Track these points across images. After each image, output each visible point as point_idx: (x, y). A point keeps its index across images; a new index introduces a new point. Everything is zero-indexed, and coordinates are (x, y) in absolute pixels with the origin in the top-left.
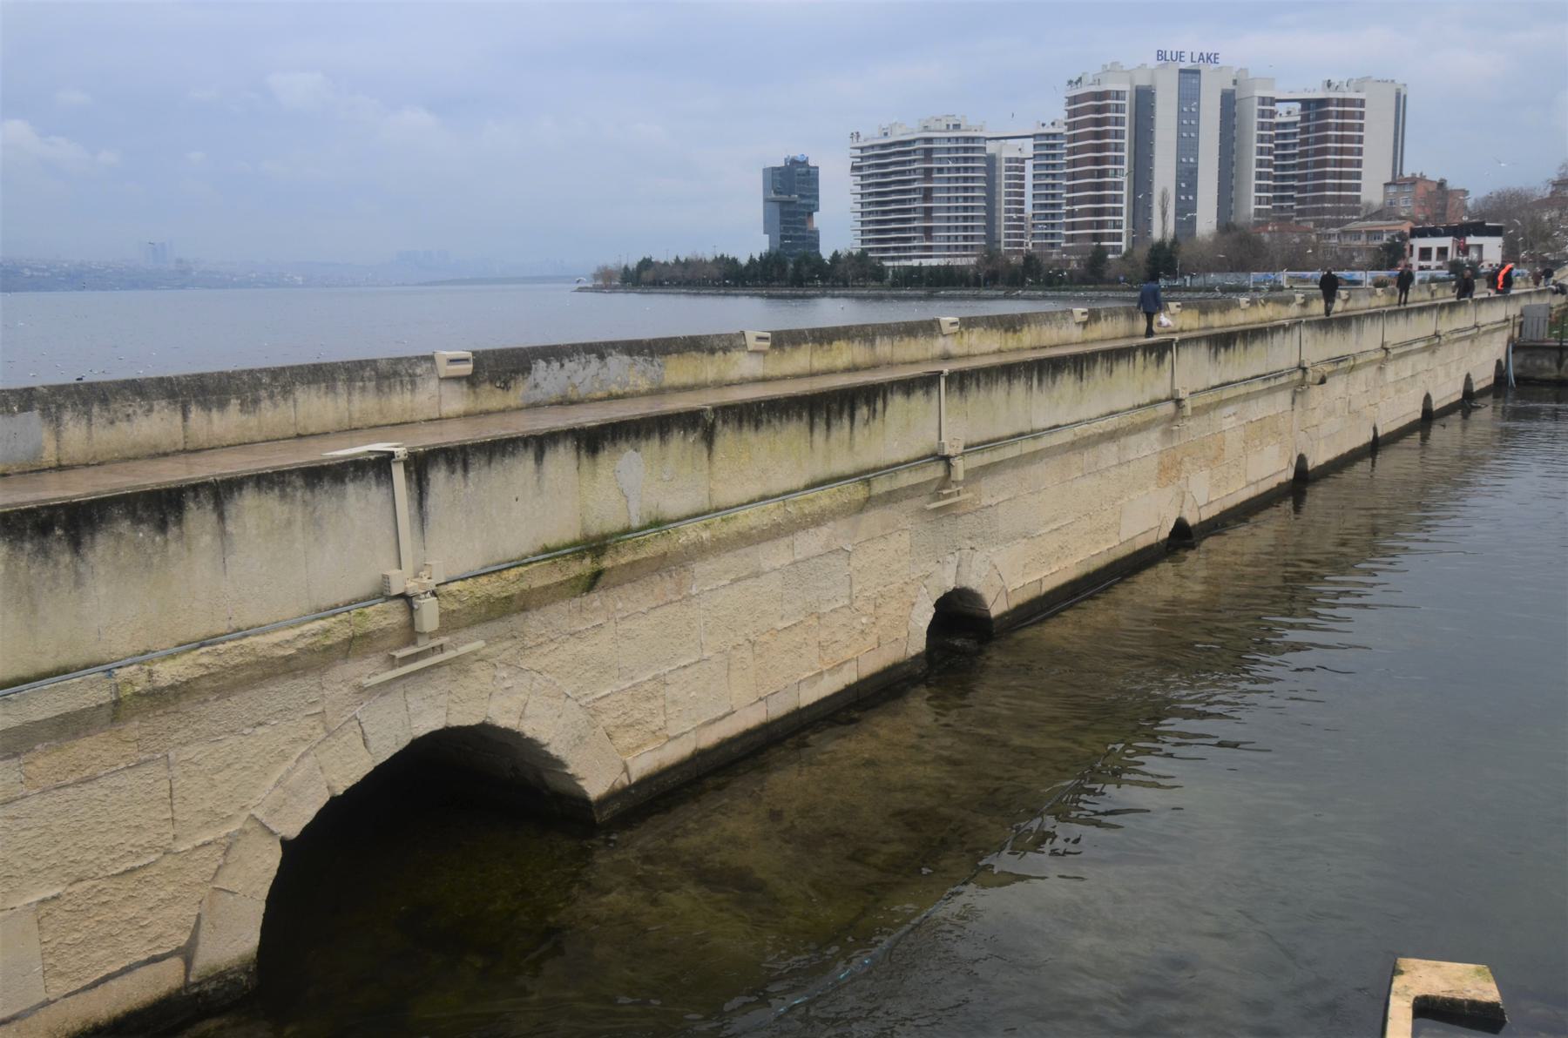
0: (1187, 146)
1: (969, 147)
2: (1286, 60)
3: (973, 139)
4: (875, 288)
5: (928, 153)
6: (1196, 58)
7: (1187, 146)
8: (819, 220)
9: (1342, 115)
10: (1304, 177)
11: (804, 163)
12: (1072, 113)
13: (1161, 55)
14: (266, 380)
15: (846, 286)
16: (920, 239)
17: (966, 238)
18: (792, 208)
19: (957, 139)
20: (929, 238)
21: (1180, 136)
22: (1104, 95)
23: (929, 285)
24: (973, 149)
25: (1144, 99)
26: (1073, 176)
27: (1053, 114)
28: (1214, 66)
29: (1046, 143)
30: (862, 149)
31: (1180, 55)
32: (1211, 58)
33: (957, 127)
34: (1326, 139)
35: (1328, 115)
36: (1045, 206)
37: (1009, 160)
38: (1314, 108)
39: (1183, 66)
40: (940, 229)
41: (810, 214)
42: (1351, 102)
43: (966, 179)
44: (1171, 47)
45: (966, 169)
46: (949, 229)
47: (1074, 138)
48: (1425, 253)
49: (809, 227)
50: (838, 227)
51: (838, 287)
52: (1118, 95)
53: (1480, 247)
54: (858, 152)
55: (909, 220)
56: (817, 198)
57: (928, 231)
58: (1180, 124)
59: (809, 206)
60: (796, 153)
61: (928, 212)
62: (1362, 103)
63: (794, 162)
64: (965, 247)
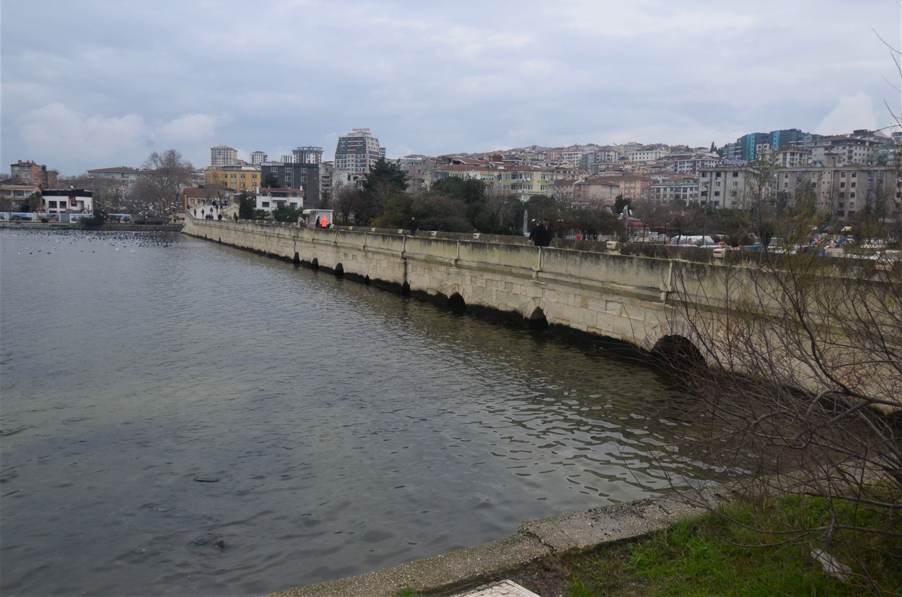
53: (82, 202)
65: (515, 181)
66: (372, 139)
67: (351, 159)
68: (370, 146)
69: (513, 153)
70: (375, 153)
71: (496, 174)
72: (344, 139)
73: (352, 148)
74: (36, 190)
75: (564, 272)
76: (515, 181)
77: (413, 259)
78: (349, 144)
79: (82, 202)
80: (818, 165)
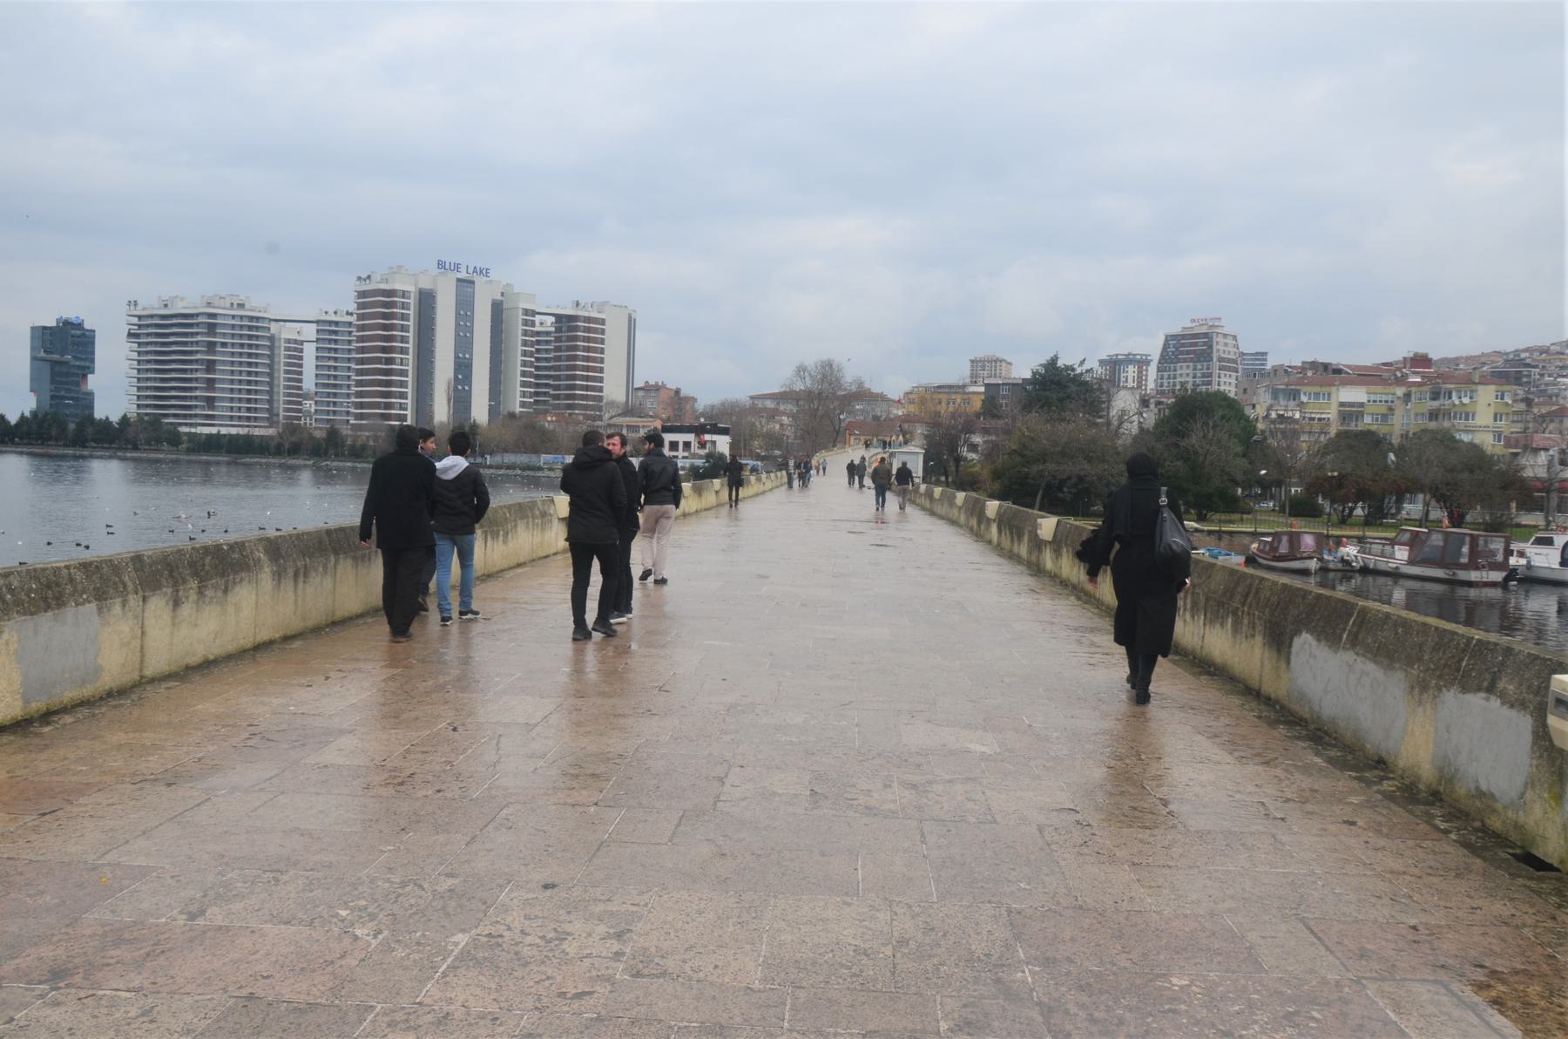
0: (464, 342)
1: (253, 329)
2: (547, 282)
3: (258, 319)
4: (170, 452)
5: (212, 328)
7: (464, 342)
8: (93, 382)
9: (588, 330)
10: (558, 378)
11: (79, 326)
12: (361, 306)
15: (136, 448)
16: (203, 408)
17: (249, 410)
18: (64, 369)
20: (212, 407)
21: (457, 335)
22: (391, 293)
23: (229, 452)
24: (257, 328)
25: (427, 300)
26: (362, 361)
27: (341, 302)
29: (329, 330)
30: (140, 317)
31: (457, 267)
32: (484, 272)
33: (241, 306)
34: (576, 348)
35: (576, 329)
36: (328, 386)
37: (288, 341)
38: (565, 322)
39: (460, 276)
40: (222, 399)
41: (85, 376)
42: (596, 321)
46: (232, 400)
47: (362, 328)
48: (674, 446)
49: (83, 388)
50: (113, 390)
51: (126, 449)
52: (404, 294)
53: (714, 443)
54: (135, 320)
55: (191, 389)
56: (93, 361)
57: (210, 402)
58: (458, 325)
59: (83, 368)
60: (71, 314)
61: (211, 383)
62: (603, 322)
63: (67, 323)
64: (248, 419)
65: (1436, 404)
66: (1225, 336)
67: (1185, 371)
68: (1220, 348)
69: (1523, 355)
70: (1229, 360)
71: (1400, 391)
72: (1173, 337)
73: (1188, 353)
74: (658, 424)
75: (121, 986)
76: (1436, 404)
77: (141, 670)
78: (1183, 345)
79: (714, 443)
80: (602, 989)
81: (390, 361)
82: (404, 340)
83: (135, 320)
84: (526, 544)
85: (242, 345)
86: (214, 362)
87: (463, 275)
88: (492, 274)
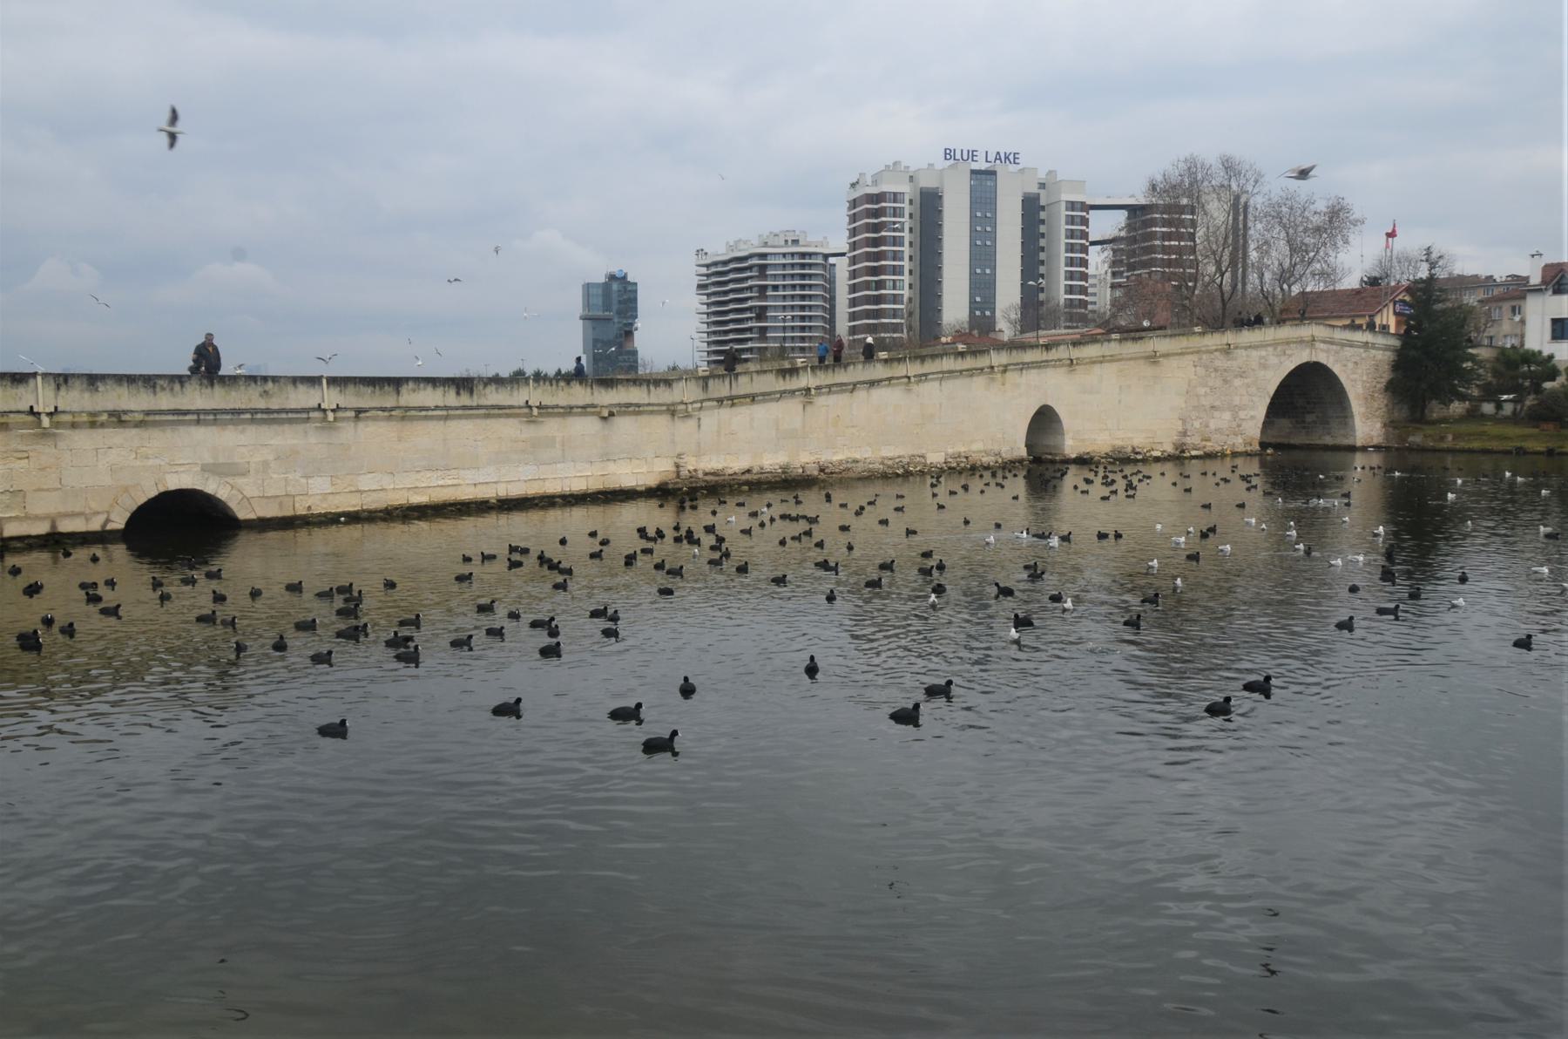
3: (810, 255)
6: (991, 157)
13: (948, 154)
14: (1517, 318)
19: (793, 254)
21: (973, 245)
22: (879, 197)
25: (930, 204)
28: (1012, 168)
30: (708, 266)
31: (972, 154)
33: (795, 242)
39: (975, 166)
43: (803, 297)
44: (961, 145)
45: (803, 287)
52: (896, 197)
54: (704, 270)
58: (973, 231)
60: (614, 270)
81: (880, 285)
82: (896, 256)
83: (704, 270)
84: (544, 640)
85: (794, 287)
86: (766, 308)
87: (982, 166)
88: (1024, 161)
